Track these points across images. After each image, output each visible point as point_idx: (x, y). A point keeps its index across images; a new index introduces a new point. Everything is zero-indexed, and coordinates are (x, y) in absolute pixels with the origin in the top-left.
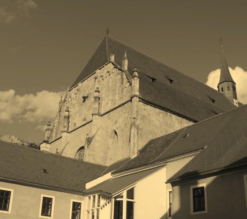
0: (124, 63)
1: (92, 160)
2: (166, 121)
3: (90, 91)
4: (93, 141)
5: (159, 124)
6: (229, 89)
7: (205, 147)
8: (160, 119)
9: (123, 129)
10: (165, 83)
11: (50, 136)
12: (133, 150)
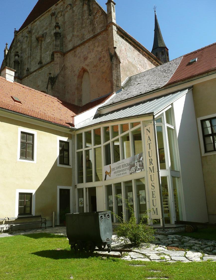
0: (141, 116)
3: (45, 31)
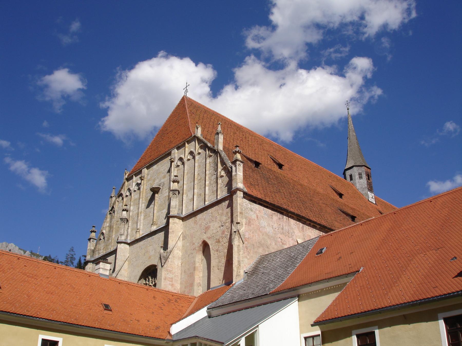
1: (170, 286)
2: (282, 226)
3: (163, 181)
4: (170, 257)
5: (272, 231)
6: (361, 177)
7: (361, 270)
8: (273, 224)
9: (219, 240)
10: (273, 169)
11: (95, 249)
12: (237, 271)
